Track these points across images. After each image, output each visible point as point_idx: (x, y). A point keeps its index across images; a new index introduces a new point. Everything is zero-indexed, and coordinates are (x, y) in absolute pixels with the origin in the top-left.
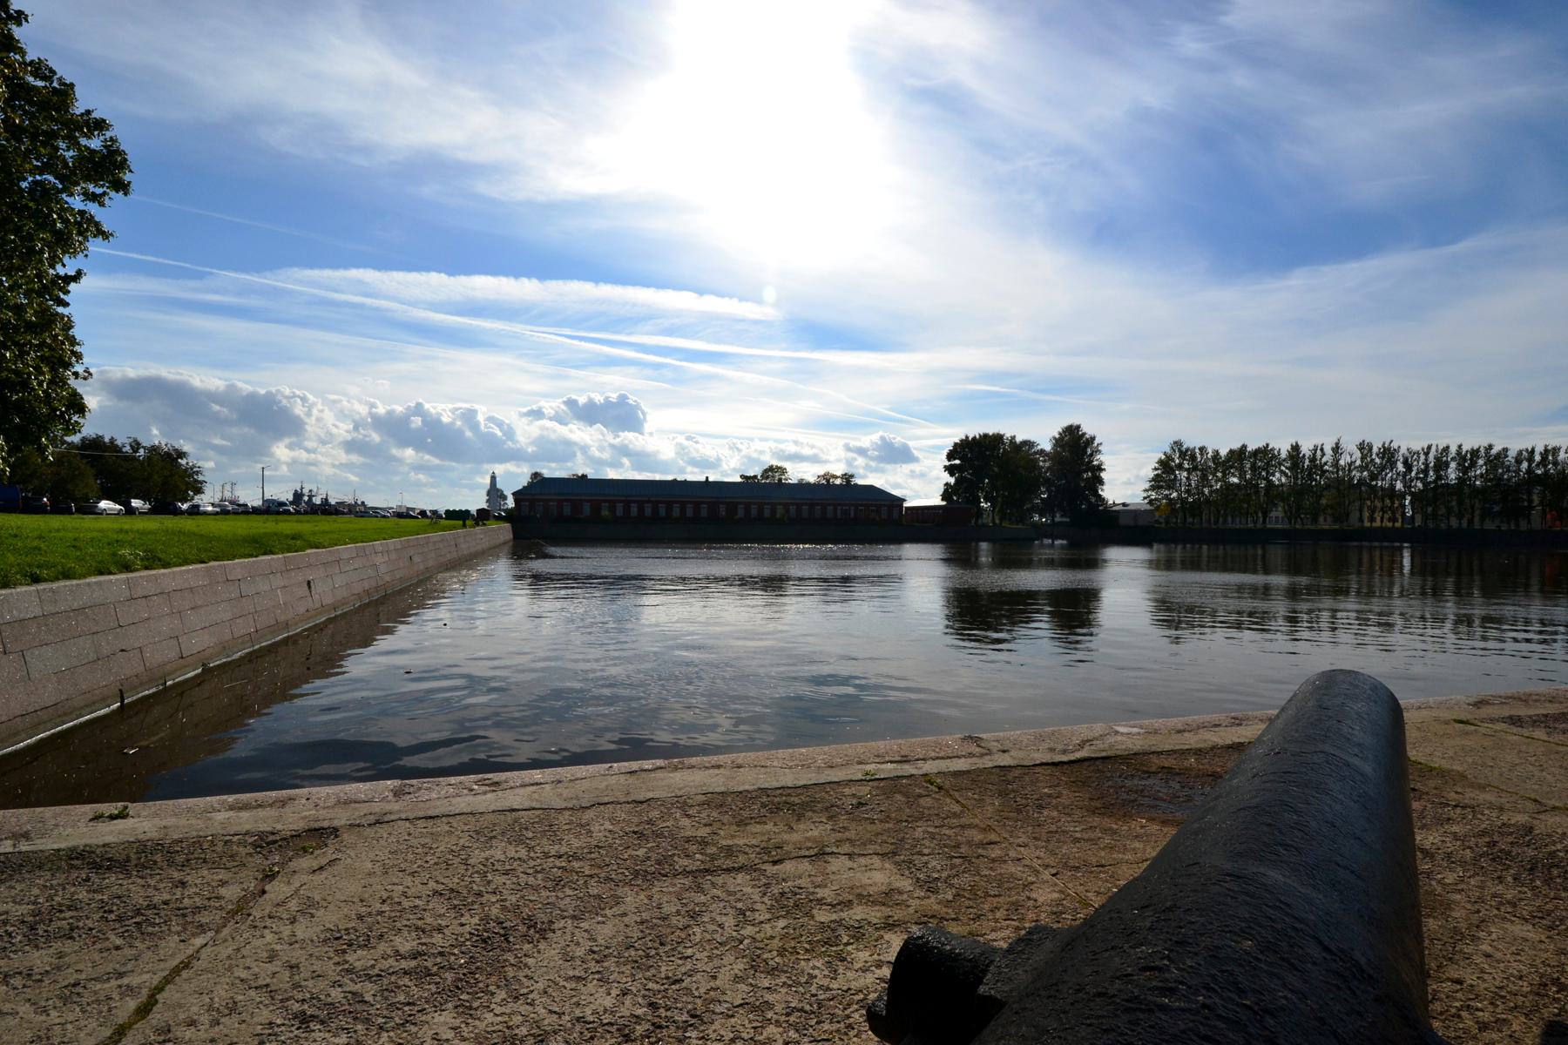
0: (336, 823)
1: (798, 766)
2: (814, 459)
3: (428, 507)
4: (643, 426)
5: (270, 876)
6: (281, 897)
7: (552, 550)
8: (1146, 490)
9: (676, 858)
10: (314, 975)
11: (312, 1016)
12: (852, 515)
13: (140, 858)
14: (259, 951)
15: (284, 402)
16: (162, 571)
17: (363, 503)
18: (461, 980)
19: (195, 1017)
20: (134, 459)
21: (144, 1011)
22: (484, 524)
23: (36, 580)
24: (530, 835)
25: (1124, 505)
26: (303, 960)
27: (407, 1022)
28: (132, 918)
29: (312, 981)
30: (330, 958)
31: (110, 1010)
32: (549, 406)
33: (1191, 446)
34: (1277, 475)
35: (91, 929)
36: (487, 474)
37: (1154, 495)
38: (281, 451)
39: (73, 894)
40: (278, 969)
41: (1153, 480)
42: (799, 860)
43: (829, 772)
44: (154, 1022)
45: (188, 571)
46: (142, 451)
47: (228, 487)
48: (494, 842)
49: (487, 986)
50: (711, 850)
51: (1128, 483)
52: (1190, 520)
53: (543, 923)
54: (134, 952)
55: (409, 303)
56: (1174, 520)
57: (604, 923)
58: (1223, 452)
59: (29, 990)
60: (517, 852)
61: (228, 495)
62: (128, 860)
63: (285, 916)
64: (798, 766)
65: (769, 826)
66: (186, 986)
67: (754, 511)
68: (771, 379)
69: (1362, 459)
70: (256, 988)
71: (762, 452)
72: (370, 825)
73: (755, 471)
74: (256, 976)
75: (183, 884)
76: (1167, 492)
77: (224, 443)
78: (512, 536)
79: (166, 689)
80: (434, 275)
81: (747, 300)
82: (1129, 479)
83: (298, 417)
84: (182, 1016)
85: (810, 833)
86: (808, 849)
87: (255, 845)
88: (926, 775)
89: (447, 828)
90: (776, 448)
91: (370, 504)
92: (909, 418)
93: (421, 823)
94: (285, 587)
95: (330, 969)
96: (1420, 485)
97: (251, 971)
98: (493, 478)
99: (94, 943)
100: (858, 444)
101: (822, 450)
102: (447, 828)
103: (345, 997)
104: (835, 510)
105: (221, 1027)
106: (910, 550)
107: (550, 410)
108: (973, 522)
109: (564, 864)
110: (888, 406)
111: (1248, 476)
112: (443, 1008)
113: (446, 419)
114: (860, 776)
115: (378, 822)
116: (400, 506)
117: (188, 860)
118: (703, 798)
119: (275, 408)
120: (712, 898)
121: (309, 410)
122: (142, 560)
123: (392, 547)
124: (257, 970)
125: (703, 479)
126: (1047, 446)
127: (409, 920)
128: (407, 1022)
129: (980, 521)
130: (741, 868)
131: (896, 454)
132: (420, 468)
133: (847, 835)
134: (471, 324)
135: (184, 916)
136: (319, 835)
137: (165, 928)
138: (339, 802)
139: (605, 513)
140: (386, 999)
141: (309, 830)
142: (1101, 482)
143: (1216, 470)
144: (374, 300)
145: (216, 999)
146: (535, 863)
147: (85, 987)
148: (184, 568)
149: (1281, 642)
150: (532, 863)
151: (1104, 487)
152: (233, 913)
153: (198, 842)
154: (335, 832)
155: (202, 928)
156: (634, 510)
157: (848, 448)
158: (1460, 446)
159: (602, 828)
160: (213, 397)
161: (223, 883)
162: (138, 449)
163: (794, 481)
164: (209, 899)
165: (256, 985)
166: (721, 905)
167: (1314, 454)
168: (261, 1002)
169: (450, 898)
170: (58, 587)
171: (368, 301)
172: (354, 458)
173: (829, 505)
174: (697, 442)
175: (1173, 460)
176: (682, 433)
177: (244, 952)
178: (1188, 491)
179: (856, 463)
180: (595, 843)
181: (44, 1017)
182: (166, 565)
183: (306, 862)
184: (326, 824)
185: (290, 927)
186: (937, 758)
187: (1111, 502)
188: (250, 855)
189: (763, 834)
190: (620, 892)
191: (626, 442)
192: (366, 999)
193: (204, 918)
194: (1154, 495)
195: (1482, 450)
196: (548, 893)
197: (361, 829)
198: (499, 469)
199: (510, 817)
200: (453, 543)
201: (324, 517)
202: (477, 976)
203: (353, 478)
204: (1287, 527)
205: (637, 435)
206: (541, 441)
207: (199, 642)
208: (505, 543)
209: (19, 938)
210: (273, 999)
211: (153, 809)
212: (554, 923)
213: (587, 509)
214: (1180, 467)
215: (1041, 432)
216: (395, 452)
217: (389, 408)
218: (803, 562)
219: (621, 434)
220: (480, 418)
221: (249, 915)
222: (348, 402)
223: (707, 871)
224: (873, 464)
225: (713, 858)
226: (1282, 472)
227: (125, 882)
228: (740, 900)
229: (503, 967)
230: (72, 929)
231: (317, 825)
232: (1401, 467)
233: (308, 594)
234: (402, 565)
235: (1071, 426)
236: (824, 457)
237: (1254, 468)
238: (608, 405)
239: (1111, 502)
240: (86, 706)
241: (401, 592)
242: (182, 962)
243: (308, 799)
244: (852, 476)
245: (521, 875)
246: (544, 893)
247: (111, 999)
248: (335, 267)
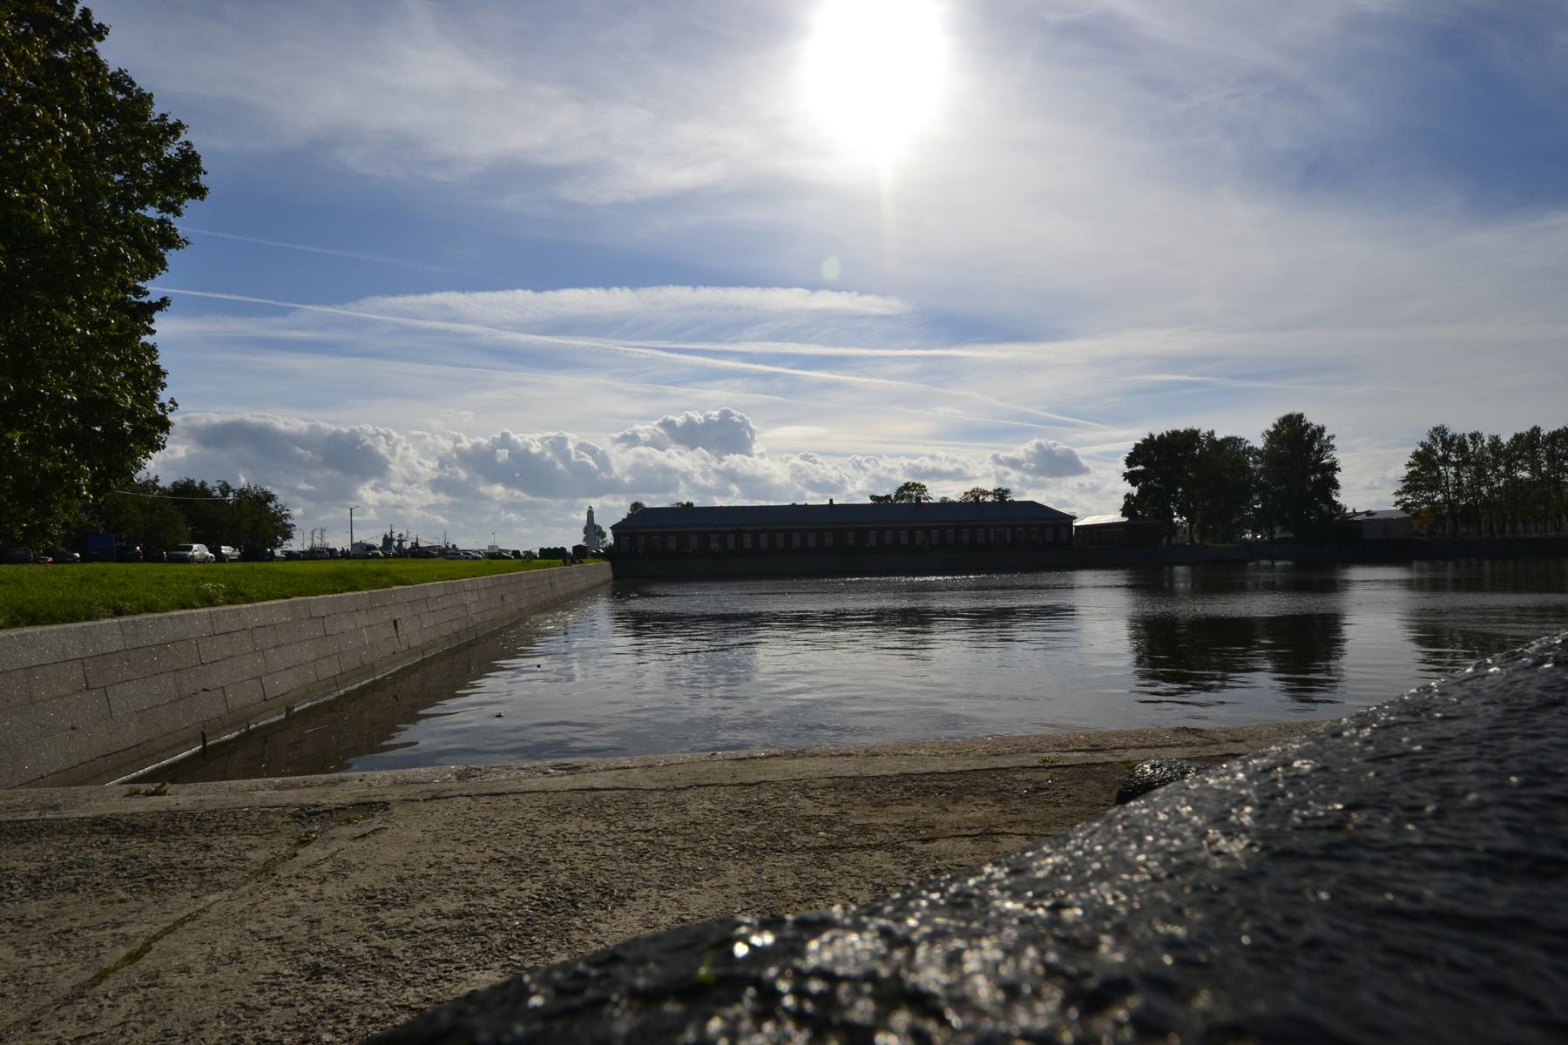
0: (389, 798)
1: (952, 754)
2: (957, 475)
3: (522, 549)
4: (750, 447)
5: (304, 842)
6: (314, 859)
7: (656, 589)
9: (793, 835)
10: (337, 930)
11: (326, 968)
12: (1009, 539)
13: (166, 825)
14: (277, 906)
15: (369, 442)
16: (244, 606)
17: (454, 546)
18: (513, 941)
19: (190, 965)
20: (225, 503)
21: (133, 958)
22: (581, 562)
23: (119, 612)
24: (612, 811)
25: (1368, 513)
26: (326, 915)
27: (441, 978)
28: (145, 875)
29: (333, 936)
30: (357, 915)
31: (98, 955)
32: (644, 429)
33: (1459, 433)
35: (98, 884)
36: (582, 509)
37: (1409, 499)
38: (367, 493)
39: (87, 854)
40: (295, 923)
41: (1408, 478)
42: (958, 839)
43: (991, 759)
44: (143, 967)
45: (272, 605)
46: (231, 494)
47: (317, 534)
48: (568, 817)
49: (546, 948)
50: (839, 828)
51: (1372, 487)
52: (1463, 529)
53: (621, 891)
54: (139, 905)
55: (495, 326)
56: (1441, 531)
57: (698, 893)
58: (1505, 439)
59: (15, 934)
60: (594, 826)
61: (317, 542)
62: (154, 826)
63: (314, 876)
64: (952, 754)
65: (917, 807)
66: (186, 936)
67: (888, 538)
68: (901, 383)
70: (267, 940)
71: (892, 471)
72: (426, 800)
73: (888, 491)
74: (269, 929)
75: (208, 847)
77: (310, 487)
78: (611, 576)
79: (249, 733)
80: (520, 292)
81: (868, 293)
82: (1372, 483)
83: (382, 457)
84: (176, 963)
85: (971, 815)
86: (969, 828)
87: (294, 816)
88: (1128, 762)
89: (514, 804)
90: (910, 464)
91: (461, 547)
92: (1075, 420)
93: (485, 799)
94: (370, 626)
95: (358, 925)
97: (264, 925)
98: (590, 513)
99: (98, 896)
100: (1010, 455)
101: (965, 464)
102: (514, 804)
103: (369, 952)
105: (218, 974)
106: (1084, 577)
107: (646, 435)
108: (1164, 541)
109: (651, 838)
110: (1043, 407)
111: (1544, 469)
112: (488, 966)
113: (535, 450)
114: (1036, 763)
115: (435, 798)
116: (492, 547)
117: (218, 827)
118: (830, 781)
119: (358, 448)
120: (841, 873)
121: (394, 448)
122: (225, 594)
123: (481, 585)
124: (271, 923)
125: (827, 502)
126: (1259, 443)
127: (457, 883)
128: (441, 978)
129: (1174, 541)
130: (881, 845)
131: (1060, 464)
132: (511, 506)
133: (1023, 816)
134: (561, 344)
135: (202, 875)
136: (367, 807)
137: (178, 885)
138: (395, 783)
139: (714, 545)
140: (419, 955)
141: (357, 804)
142: (1336, 485)
143: (1497, 463)
144: (459, 325)
145: (219, 949)
146: (614, 836)
147: (76, 934)
148: (266, 603)
150: (611, 836)
151: (1340, 491)
152: (255, 874)
153: (233, 812)
154: (385, 805)
155: (220, 886)
156: (748, 541)
157: (997, 460)
159: (701, 807)
160: (297, 439)
161: (252, 847)
162: (228, 492)
164: (233, 860)
165: (268, 936)
166: (853, 880)
168: (269, 953)
169: (509, 865)
170: (141, 621)
171: (453, 326)
172: (443, 498)
174: (815, 462)
176: (796, 453)
177: (260, 906)
178: (1458, 492)
179: (1008, 478)
180: (692, 820)
181: (25, 960)
182: (249, 600)
183: (347, 831)
184: (377, 799)
185: (318, 886)
186: (1142, 747)
187: (1349, 511)
188: (288, 823)
189: (907, 814)
190: (720, 865)
191: (733, 466)
192: (395, 954)
193: (224, 877)
194: (1409, 499)
196: (629, 864)
197: (416, 804)
198: (596, 503)
199: (589, 796)
200: (547, 581)
201: (412, 560)
202: (533, 938)
203: (442, 520)
205: (745, 457)
206: (635, 470)
207: (281, 685)
208: (605, 583)
209: (20, 890)
210: (284, 950)
211: (193, 789)
212: (634, 891)
213: (694, 542)
214: (1445, 460)
216: (482, 489)
217: (474, 441)
219: (725, 457)
220: (571, 446)
221: (274, 875)
222: (433, 437)
223: (833, 847)
224: (1029, 478)
225: (842, 835)
227: (145, 845)
228: (878, 876)
229: (567, 930)
230: (77, 884)
231: (366, 800)
233: (395, 635)
234: (493, 605)
236: (970, 473)
237: (1551, 457)
238: (709, 424)
239: (1349, 511)
240: (168, 748)
241: (493, 634)
242: (189, 915)
243: (361, 780)
244: (1007, 491)
245: (597, 847)
246: (624, 864)
247: (102, 946)
248: (418, 291)
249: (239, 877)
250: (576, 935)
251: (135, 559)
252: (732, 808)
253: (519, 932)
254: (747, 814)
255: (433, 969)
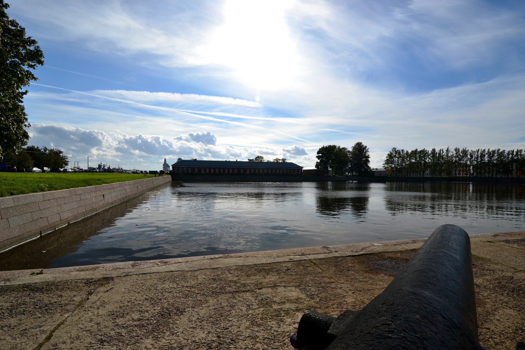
0: (112, 276)
1: (267, 256)
2: (273, 154)
3: (143, 170)
4: (215, 143)
5: (90, 293)
7: (185, 184)
8: (384, 164)
9: (226, 287)
10: (105, 326)
11: (104, 340)
12: (285, 172)
13: (47, 288)
14: (87, 319)
15: (95, 135)
16: (54, 191)
17: (122, 168)
18: (154, 328)
19: (65, 341)
20: (45, 154)
21: (48, 339)
22: (162, 176)
23: (12, 194)
24: (178, 280)
25: (376, 169)
26: (101, 322)
27: (136, 342)
28: (44, 307)
30: (110, 321)
31: (37, 338)
32: (184, 136)
33: (399, 150)
34: (428, 159)
35: (30, 311)
36: (163, 159)
37: (386, 166)
38: (94, 151)
40: (93, 325)
41: (386, 161)
42: (268, 288)
44: (52, 342)
45: (63, 191)
47: (76, 163)
48: (165, 282)
49: (163, 330)
50: (238, 285)
51: (378, 162)
52: (398, 174)
53: (182, 309)
54: (45, 319)
55: (137, 102)
56: (393, 174)
57: (202, 309)
58: (410, 151)
59: (10, 332)
61: (76, 166)
62: (43, 288)
63: (95, 307)
64: (267, 256)
65: (258, 277)
66: (62, 330)
67: (252, 171)
68: (258, 127)
69: (456, 154)
70: (86, 331)
71: (255, 152)
72: (124, 276)
73: (253, 158)
74: (86, 327)
75: (61, 296)
76: (391, 165)
77: (75, 148)
78: (171, 180)
79: (56, 231)
80: (145, 92)
82: (378, 160)
83: (100, 140)
84: (61, 340)
86: (271, 284)
87: (85, 283)
89: (150, 277)
90: (260, 150)
91: (124, 169)
92: (304, 140)
93: (141, 276)
94: (95, 197)
96: (475, 162)
97: (84, 325)
98: (165, 160)
99: (31, 316)
100: (287, 149)
101: (275, 151)
102: (150, 277)
103: (116, 334)
104: (280, 171)
105: (74, 344)
106: (305, 184)
107: (184, 137)
108: (326, 175)
109: (189, 289)
110: (297, 136)
111: (418, 160)
112: (148, 337)
113: (149, 140)
114: (288, 260)
115: (127, 275)
116: (134, 170)
117: (63, 288)
118: (235, 267)
119: (92, 137)
121: (104, 137)
122: (48, 187)
123: (131, 183)
124: (86, 325)
125: (236, 160)
126: (351, 149)
127: (137, 308)
128: (136, 342)
129: (328, 175)
130: (248, 291)
131: (300, 152)
132: (141, 157)
133: (284, 280)
134: (158, 109)
135: (62, 307)
136: (107, 280)
137: (55, 311)
138: (113, 269)
139: (203, 172)
140: (129, 334)
141: (103, 278)
142: (369, 161)
143: (407, 157)
144: (125, 101)
145: (72, 335)
146: (179, 289)
147: (28, 331)
148: (61, 190)
149: (429, 215)
150: (178, 289)
151: (370, 163)
153: (66, 282)
154: (112, 279)
155: (68, 311)
156: (212, 171)
157: (284, 150)
158: (489, 150)
159: (202, 277)
160: (71, 133)
161: (75, 296)
162: (46, 150)
163: (266, 161)
164: (70, 301)
165: (86, 330)
166: (242, 303)
167: (440, 152)
168: (87, 336)
169: (151, 301)
170: (20, 197)
171: (123, 101)
172: (119, 153)
173: (278, 169)
174: (233, 148)
175: (393, 154)
176: (228, 145)
177: (82, 319)
178: (398, 165)
179: (287, 155)
180: (199, 282)
181: (15, 341)
182: (56, 189)
183: (102, 289)
184: (109, 276)
185: (97, 310)
186: (314, 254)
187: (372, 168)
188: (84, 286)
189: (255, 279)
190: (207, 299)
191: (210, 148)
192: (123, 334)
193: (68, 307)
194: (386, 166)
195: (496, 151)
196: (184, 299)
197: (121, 278)
198: (167, 157)
199: (171, 274)
200: (152, 182)
201: (108, 173)
202: (160, 327)
203: (118, 160)
204: (431, 176)
205: (213, 146)
206: (181, 148)
207: (67, 215)
208: (169, 182)
209: (6, 314)
210: (91, 335)
211: (51, 271)
212: (185, 309)
213: (196, 170)
214: (395, 156)
215: (349, 145)
216: (132, 151)
217: (130, 137)
218: (269, 188)
219: (208, 145)
220: (161, 140)
221: (83, 306)
222: (117, 135)
223: (237, 292)
224: (292, 155)
225: (239, 287)
226: (429, 158)
227: (42, 296)
228: (248, 301)
229: (168, 324)
230: (24, 311)
231: (106, 276)
232: (469, 156)
233: (103, 199)
234: (134, 189)
235: (359, 143)
236: (276, 153)
237: (420, 157)
238: (204, 136)
239: (372, 168)
240: (29, 236)
241: (134, 198)
242: (61, 322)
243: (103, 268)
244: (285, 159)
245: (175, 293)
246: (182, 299)
247: (37, 334)
248: (112, 89)
249: (73, 307)
250: (171, 326)
251: (14, 171)
252: (210, 278)
253: (156, 325)
254: (214, 280)
255: (134, 339)
